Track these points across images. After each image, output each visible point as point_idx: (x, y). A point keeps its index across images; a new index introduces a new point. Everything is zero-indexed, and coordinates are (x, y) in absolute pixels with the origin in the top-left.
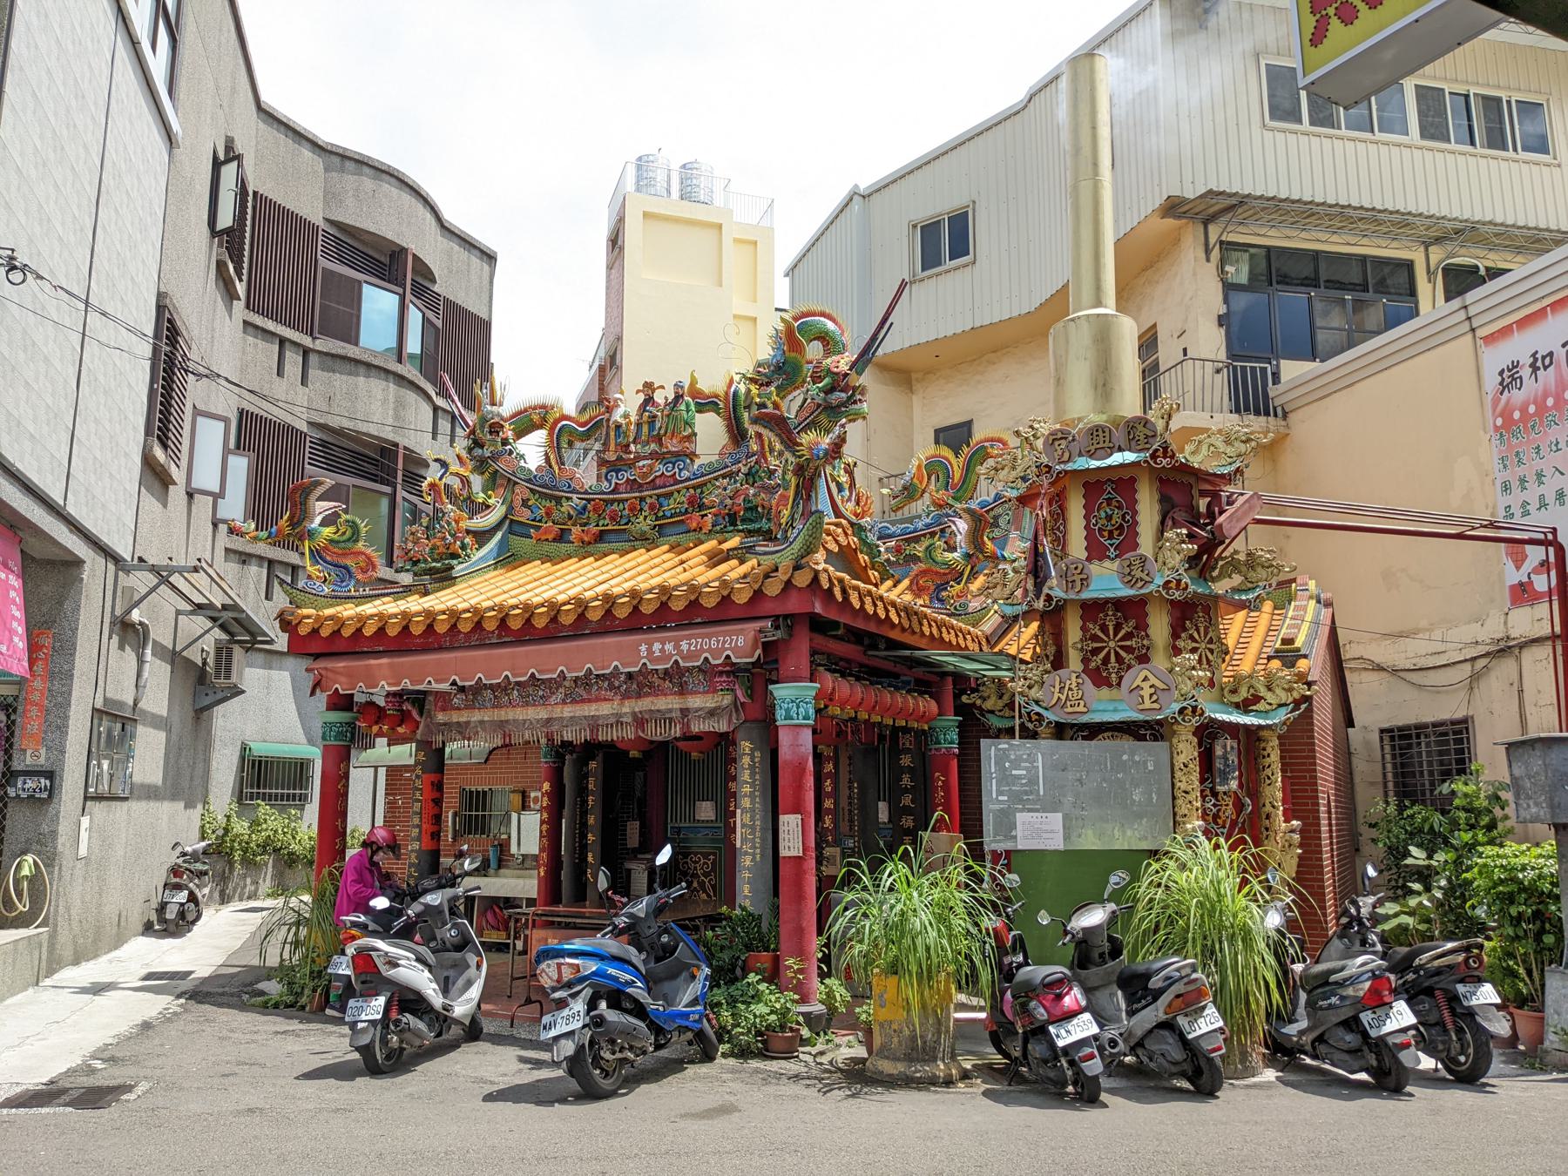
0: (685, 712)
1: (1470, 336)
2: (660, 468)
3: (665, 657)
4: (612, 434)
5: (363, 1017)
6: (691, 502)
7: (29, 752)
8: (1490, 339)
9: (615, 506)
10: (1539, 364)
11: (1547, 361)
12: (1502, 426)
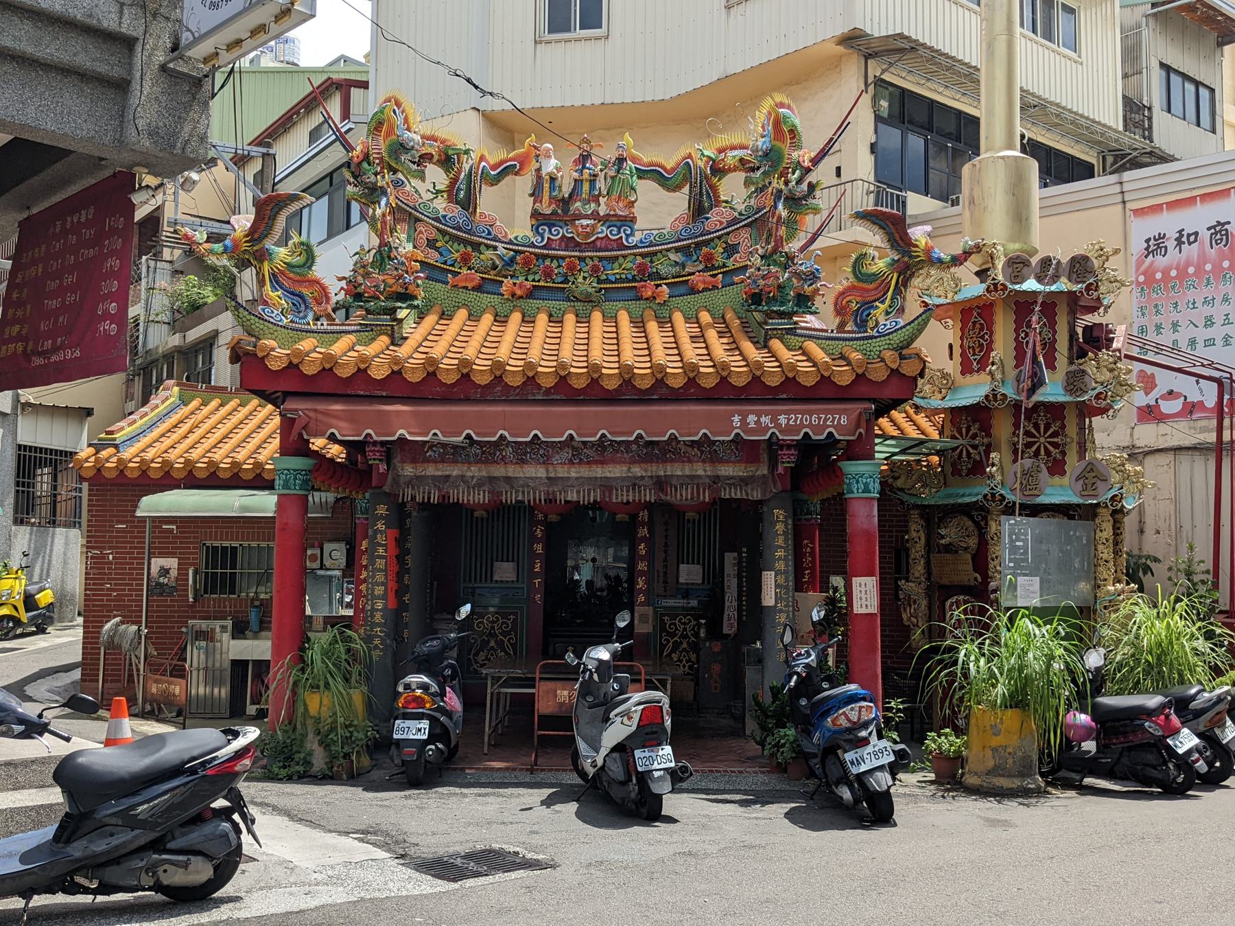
0: (716, 479)
1: (1120, 207)
2: (603, 231)
3: (761, 429)
4: (546, 186)
5: (656, 766)
6: (642, 269)
8: (1138, 212)
9: (548, 262)
10: (1184, 239)
11: (1192, 239)
12: (1144, 283)
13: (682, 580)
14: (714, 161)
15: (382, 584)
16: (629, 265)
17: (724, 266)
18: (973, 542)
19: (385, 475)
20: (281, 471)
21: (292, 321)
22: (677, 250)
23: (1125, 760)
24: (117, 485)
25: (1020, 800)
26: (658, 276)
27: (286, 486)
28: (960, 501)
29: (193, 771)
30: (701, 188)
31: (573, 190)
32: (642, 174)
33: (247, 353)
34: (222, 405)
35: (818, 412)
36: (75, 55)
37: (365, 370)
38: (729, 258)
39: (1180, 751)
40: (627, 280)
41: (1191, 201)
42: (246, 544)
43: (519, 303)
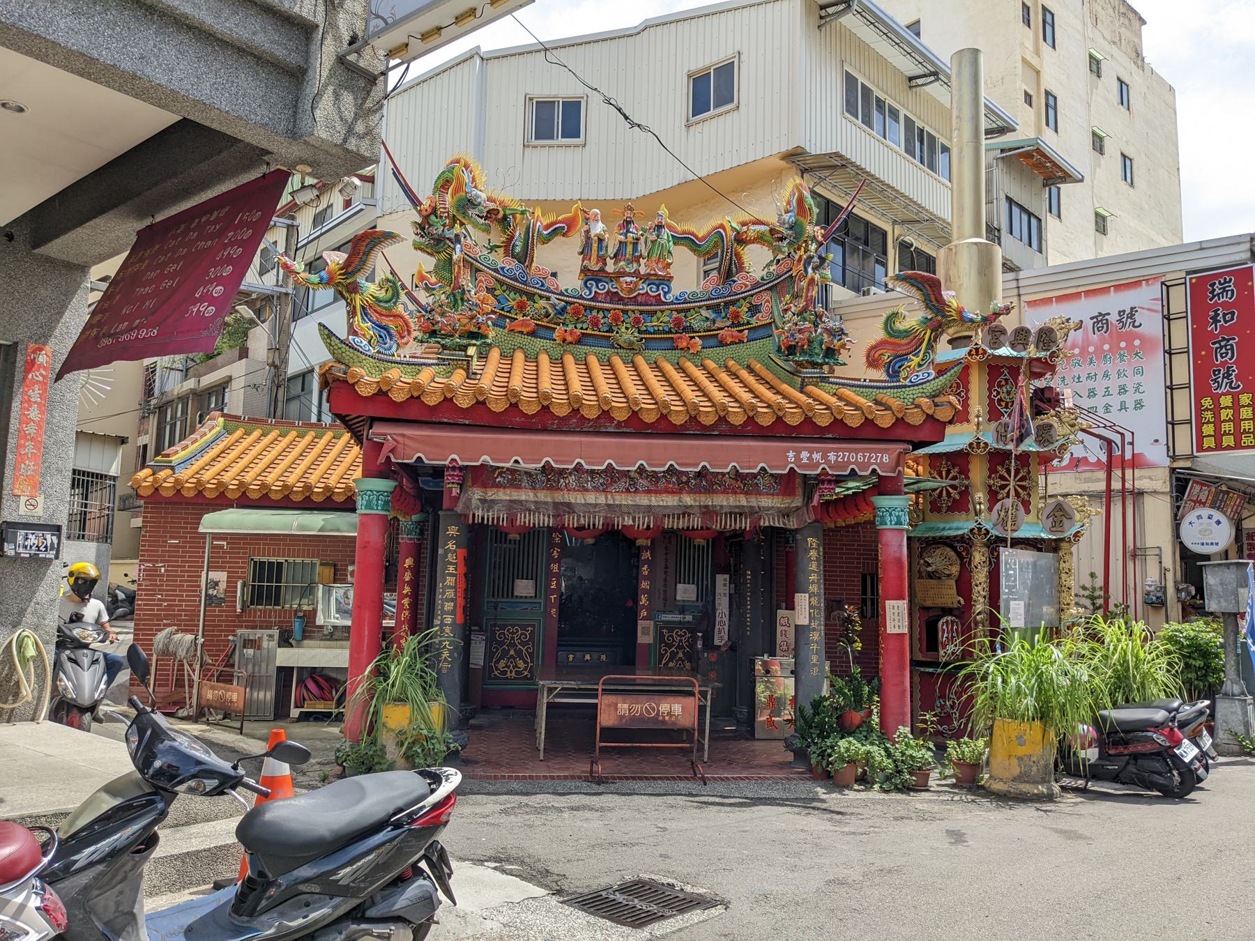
2: (644, 288)
4: (595, 246)
6: (678, 322)
7: (23, 499)
9: (594, 313)
13: (678, 598)
14: (738, 233)
15: (452, 600)
16: (665, 319)
17: (748, 323)
18: (955, 570)
19: (457, 498)
20: (365, 492)
21: (379, 352)
22: (708, 307)
23: (1132, 768)
24: (170, 503)
25: (1038, 805)
26: (690, 329)
27: (369, 506)
28: (946, 533)
29: (397, 825)
30: (722, 254)
31: (618, 250)
32: (677, 240)
33: (337, 380)
34: (264, 435)
35: (863, 451)
36: (254, 34)
37: (451, 399)
38: (752, 316)
39: (1187, 760)
40: (664, 332)
41: (1078, 295)
42: (291, 560)
43: (570, 347)
